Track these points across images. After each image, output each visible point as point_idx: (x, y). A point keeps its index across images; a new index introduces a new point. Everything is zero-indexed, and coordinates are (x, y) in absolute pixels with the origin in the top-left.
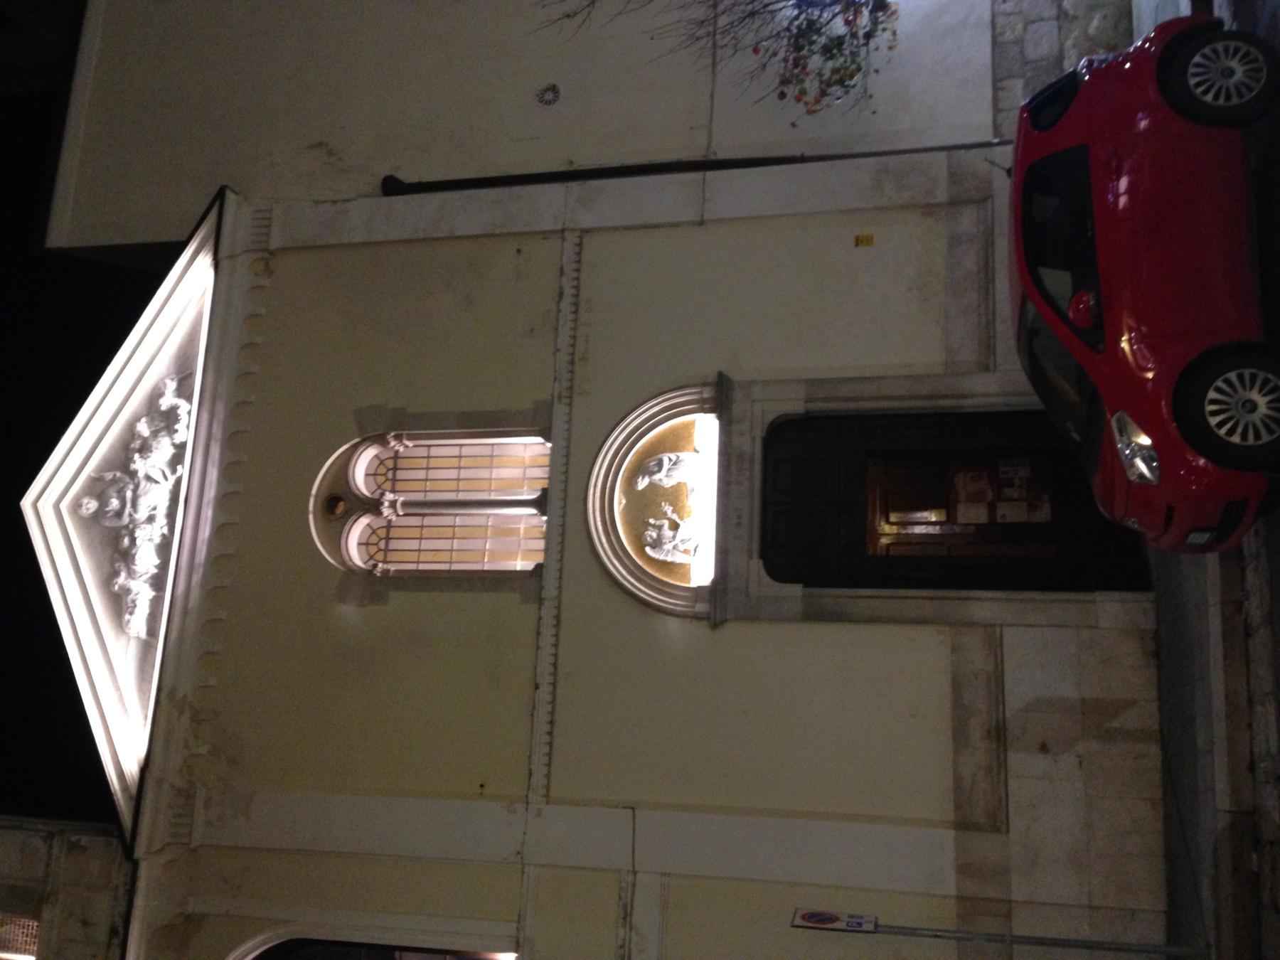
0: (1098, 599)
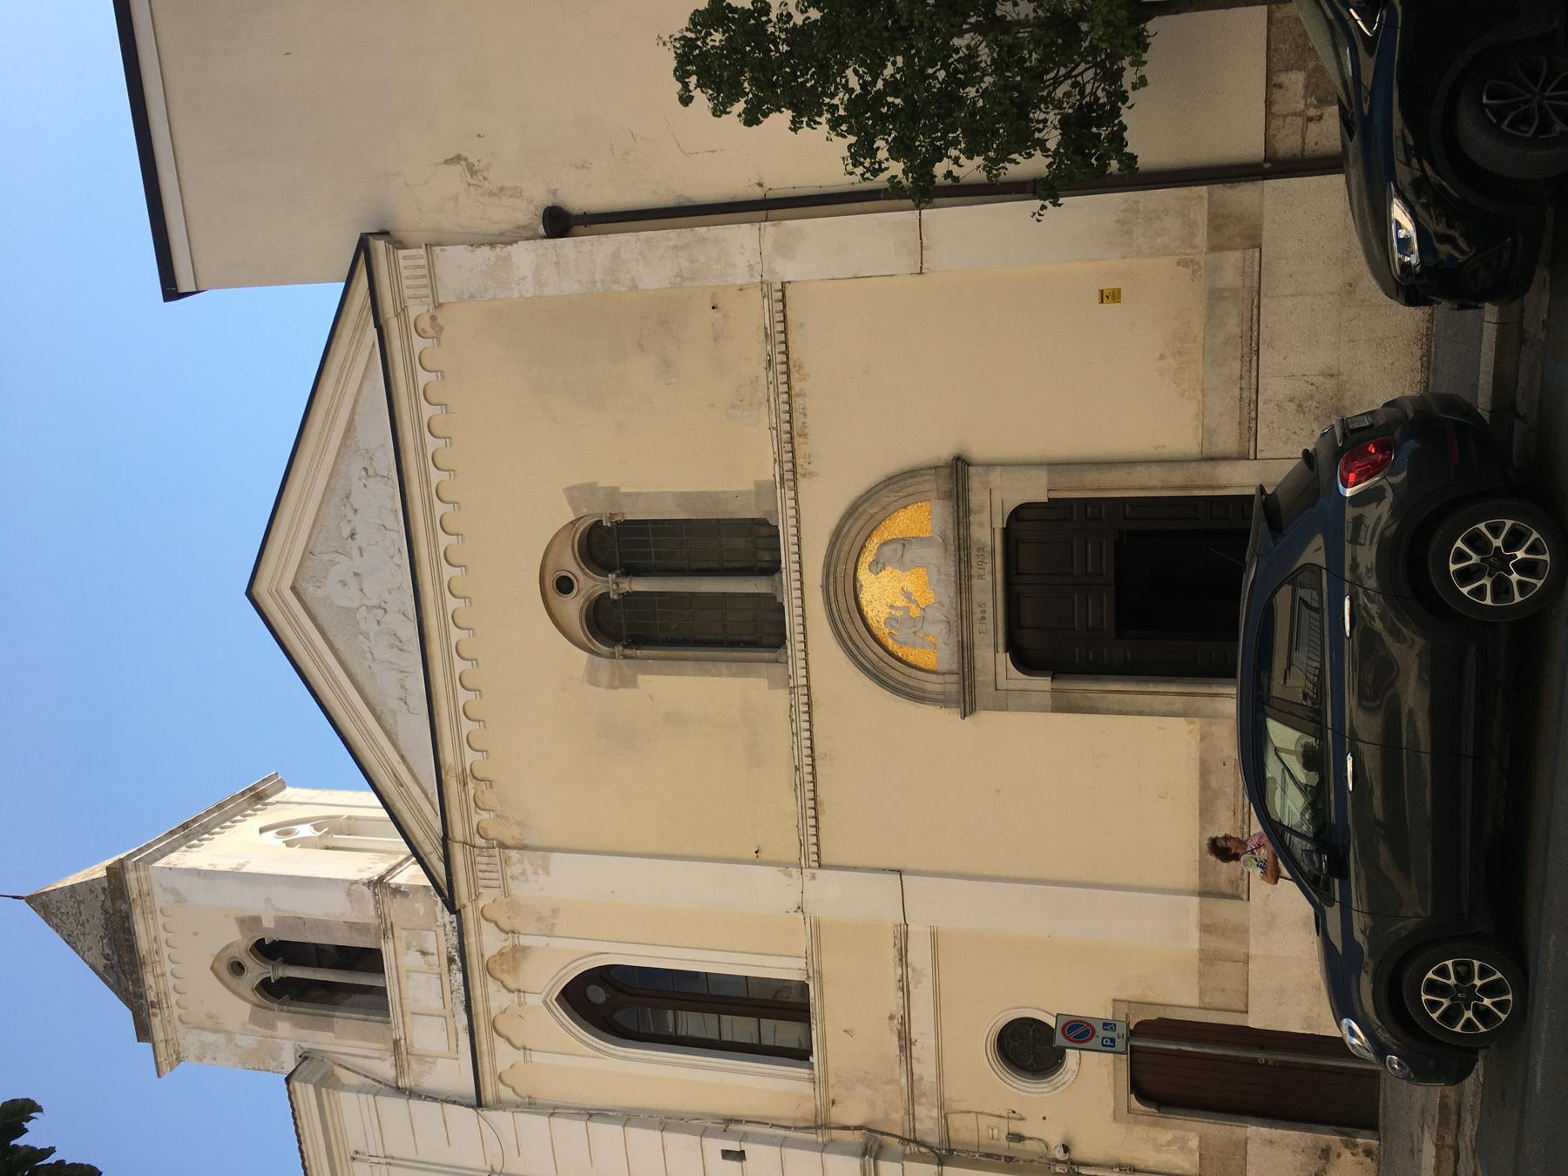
0: (1004, 1142)
